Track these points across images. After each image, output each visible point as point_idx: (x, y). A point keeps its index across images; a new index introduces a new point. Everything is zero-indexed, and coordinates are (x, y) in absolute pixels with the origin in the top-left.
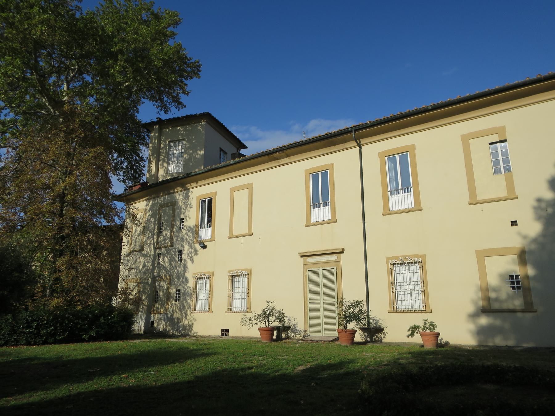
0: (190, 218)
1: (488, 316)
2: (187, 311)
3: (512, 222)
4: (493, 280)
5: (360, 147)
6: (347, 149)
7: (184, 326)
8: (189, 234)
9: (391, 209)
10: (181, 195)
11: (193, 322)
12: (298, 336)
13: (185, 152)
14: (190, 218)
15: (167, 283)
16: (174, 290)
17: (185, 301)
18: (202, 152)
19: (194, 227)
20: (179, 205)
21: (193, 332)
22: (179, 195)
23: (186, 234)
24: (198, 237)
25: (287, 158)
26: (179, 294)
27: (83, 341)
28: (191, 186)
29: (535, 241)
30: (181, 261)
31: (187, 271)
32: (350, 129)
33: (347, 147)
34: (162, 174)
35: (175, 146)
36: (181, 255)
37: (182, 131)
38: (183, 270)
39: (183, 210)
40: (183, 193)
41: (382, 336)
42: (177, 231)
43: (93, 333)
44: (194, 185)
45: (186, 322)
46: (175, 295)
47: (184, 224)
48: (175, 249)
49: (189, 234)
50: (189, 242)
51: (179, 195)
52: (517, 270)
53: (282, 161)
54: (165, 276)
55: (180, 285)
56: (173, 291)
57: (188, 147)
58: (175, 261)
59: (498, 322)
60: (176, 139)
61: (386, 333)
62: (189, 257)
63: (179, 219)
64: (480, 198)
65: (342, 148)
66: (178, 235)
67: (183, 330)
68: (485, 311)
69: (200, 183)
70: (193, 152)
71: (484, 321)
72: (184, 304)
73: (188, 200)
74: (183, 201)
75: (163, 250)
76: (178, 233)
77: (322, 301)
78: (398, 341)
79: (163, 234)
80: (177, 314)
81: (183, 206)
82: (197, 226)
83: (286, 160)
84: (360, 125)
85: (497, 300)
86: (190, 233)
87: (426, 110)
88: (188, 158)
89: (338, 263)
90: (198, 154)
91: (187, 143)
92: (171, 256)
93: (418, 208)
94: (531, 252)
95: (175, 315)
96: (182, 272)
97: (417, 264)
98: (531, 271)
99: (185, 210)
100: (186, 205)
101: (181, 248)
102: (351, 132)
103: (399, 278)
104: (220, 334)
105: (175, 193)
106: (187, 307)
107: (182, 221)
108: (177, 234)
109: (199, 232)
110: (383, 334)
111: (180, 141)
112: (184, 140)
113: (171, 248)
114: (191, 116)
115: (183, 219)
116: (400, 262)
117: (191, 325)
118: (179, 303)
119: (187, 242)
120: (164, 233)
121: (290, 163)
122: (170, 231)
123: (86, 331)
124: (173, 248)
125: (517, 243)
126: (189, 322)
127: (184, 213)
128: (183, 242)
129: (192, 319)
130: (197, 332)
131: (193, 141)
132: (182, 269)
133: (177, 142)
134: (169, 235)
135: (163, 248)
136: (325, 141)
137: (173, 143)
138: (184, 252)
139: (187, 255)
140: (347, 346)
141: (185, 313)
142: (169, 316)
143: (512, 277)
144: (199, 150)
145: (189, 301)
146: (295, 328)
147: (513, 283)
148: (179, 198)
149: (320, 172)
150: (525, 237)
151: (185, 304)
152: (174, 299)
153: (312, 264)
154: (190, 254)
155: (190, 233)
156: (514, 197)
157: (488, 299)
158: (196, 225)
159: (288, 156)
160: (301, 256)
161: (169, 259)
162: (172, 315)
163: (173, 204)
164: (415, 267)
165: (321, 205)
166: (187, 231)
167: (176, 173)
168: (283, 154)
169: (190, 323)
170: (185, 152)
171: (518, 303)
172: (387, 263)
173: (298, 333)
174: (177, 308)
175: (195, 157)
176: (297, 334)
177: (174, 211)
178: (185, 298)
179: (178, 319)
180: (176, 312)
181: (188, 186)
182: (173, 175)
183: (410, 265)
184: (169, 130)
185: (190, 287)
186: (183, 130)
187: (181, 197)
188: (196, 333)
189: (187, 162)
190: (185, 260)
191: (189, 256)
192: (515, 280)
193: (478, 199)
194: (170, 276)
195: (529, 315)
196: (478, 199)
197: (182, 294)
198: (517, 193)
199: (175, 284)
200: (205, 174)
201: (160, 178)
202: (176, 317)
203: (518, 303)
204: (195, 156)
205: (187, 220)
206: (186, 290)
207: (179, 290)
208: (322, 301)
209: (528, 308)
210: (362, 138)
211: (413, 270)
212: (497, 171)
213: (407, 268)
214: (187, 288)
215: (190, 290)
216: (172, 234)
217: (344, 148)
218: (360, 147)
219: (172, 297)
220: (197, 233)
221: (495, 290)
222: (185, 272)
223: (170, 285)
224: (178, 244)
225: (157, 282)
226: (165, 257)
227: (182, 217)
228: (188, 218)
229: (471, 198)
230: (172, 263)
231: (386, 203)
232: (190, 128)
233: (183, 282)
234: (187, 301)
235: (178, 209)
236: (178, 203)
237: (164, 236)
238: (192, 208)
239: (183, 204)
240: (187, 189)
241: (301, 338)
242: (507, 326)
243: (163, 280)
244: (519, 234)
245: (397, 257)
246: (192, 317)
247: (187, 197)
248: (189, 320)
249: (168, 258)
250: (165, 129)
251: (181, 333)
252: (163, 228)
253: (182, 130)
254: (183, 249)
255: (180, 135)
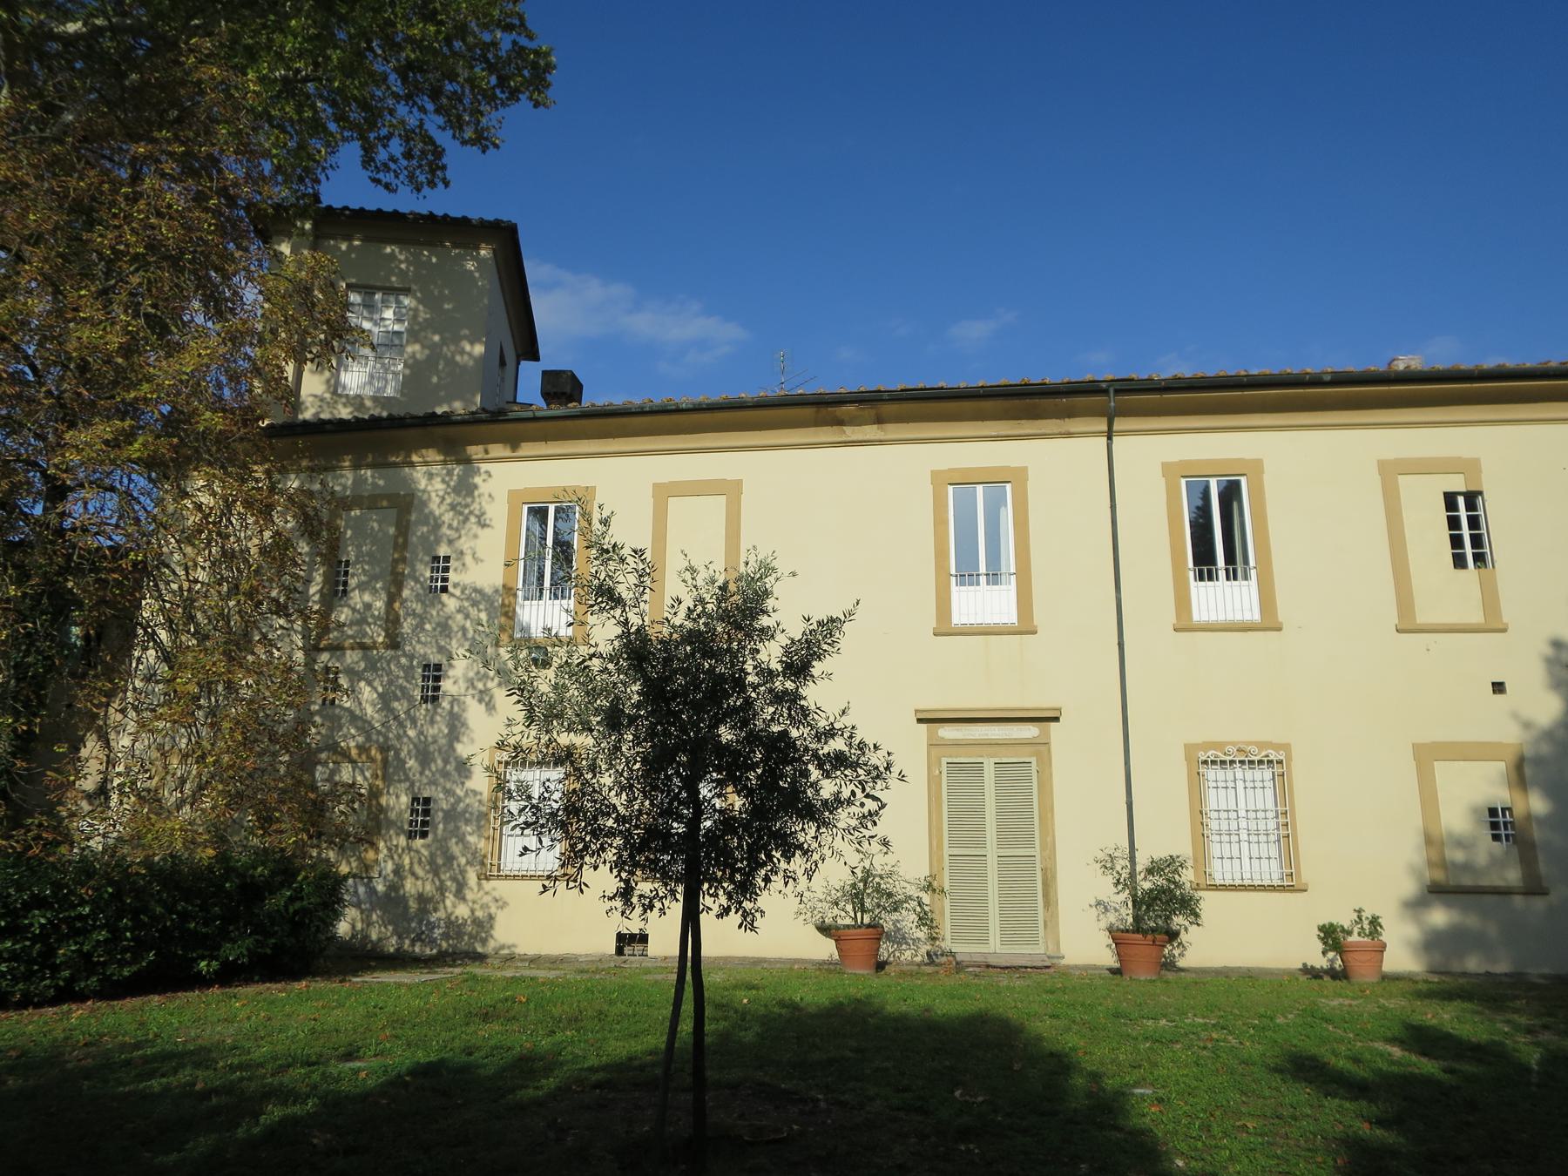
0: (476, 559)
1: (1448, 905)
2: (463, 872)
3: (1494, 684)
4: (1457, 818)
5: (1110, 438)
6: (1069, 435)
7: (450, 922)
8: (473, 612)
9: (1196, 618)
10: (439, 479)
11: (493, 910)
12: (908, 953)
13: (414, 335)
14: (476, 559)
15: (368, 774)
16: (405, 800)
17: (454, 840)
18: (479, 349)
19: (497, 591)
20: (427, 511)
21: (492, 944)
22: (430, 476)
23: (459, 611)
24: (513, 628)
25: (875, 426)
26: (426, 812)
27: (202, 982)
28: (486, 452)
29: (1548, 735)
30: (435, 699)
31: (465, 739)
32: (1104, 385)
33: (1073, 430)
34: (315, 393)
35: (369, 306)
36: (437, 679)
37: (401, 262)
38: (446, 731)
39: (445, 530)
40: (450, 473)
41: (1176, 952)
42: (418, 598)
43: (232, 952)
44: (497, 450)
45: (462, 911)
46: (407, 815)
47: (452, 575)
48: (411, 657)
49: (473, 612)
50: (473, 638)
51: (430, 476)
52: (1501, 795)
53: (851, 433)
54: (358, 747)
55: (433, 782)
56: (398, 802)
57: (426, 320)
58: (410, 699)
59: (1472, 921)
60: (378, 284)
61: (1186, 944)
62: (471, 691)
63: (427, 558)
64: (1422, 618)
65: (1056, 431)
66: (425, 612)
67: (446, 936)
68: (1437, 892)
69: (527, 449)
70: (444, 341)
71: (1439, 917)
72: (448, 849)
73: (469, 500)
74: (448, 500)
75: (352, 657)
76: (423, 603)
77: (992, 851)
78: (1238, 965)
79: (351, 602)
80: (419, 883)
81: (447, 517)
82: (509, 590)
83: (871, 431)
84: (1133, 380)
85: (1466, 867)
86: (479, 611)
87: (1316, 381)
88: (424, 357)
89: (1041, 747)
90: (462, 352)
91: (421, 308)
92: (390, 682)
93: (1269, 623)
94: (1538, 761)
95: (410, 886)
96: (443, 741)
97: (1265, 766)
98: (1537, 804)
99: (457, 530)
100: (461, 513)
101: (435, 658)
102: (1105, 392)
103: (1215, 799)
104: (610, 947)
105: (412, 465)
106: (463, 861)
107: (441, 565)
108: (419, 608)
109: (518, 609)
110: (1178, 947)
111: (389, 290)
112: (406, 291)
113: (389, 653)
114: (464, 222)
115: (447, 559)
116: (1228, 758)
117: (486, 919)
118: (427, 846)
119: (467, 639)
120: (357, 598)
121: (881, 442)
122: (384, 596)
123: (210, 946)
124: (400, 653)
125: (1511, 735)
126: (473, 911)
127: (450, 542)
128: (449, 636)
129: (487, 899)
130: (514, 946)
131: (446, 306)
132: (440, 730)
133: (378, 296)
134: (379, 610)
135: (352, 649)
136: (1016, 402)
137: (359, 293)
138: (451, 673)
139: (462, 685)
140: (1151, 981)
141: (453, 879)
142: (380, 888)
143: (1493, 812)
144: (466, 337)
145: (472, 839)
146: (899, 929)
147: (1494, 826)
148: (429, 488)
149: (981, 486)
150: (1527, 725)
151: (456, 849)
152: (403, 831)
153: (957, 744)
154: (480, 680)
155: (479, 611)
156: (1501, 627)
157: (1444, 864)
158: (504, 586)
159: (879, 420)
160: (920, 721)
161: (380, 689)
162: (394, 887)
163: (405, 505)
164: (1258, 774)
165: (983, 579)
166: (466, 604)
167: (375, 399)
168: (868, 411)
169: (479, 914)
170: (414, 335)
171: (1512, 876)
172: (1188, 759)
173: (907, 943)
174: (416, 860)
175: (451, 362)
176: (904, 947)
177: (404, 529)
178: (458, 828)
179: (422, 898)
180: (413, 874)
181: (475, 451)
182: (362, 405)
183: (1247, 767)
184: (350, 247)
185: (475, 793)
186: (407, 260)
187: (438, 485)
188: (509, 947)
189: (417, 374)
190: (454, 700)
191: (474, 687)
192: (1501, 819)
193: (1418, 622)
194: (384, 749)
195: (1539, 903)
196: (1418, 622)
197: (440, 814)
198: (1505, 620)
199: (407, 779)
200: (569, 423)
201: (308, 404)
202: (413, 891)
203: (1512, 876)
204: (453, 357)
205: (464, 565)
206: (459, 800)
207: (427, 801)
208: (992, 851)
209: (1534, 888)
210: (1119, 416)
211: (1254, 781)
212: (1459, 562)
213: (1239, 774)
214: (467, 794)
215: (480, 801)
216: (397, 605)
217: (1063, 431)
218: (1110, 438)
219: (391, 824)
220: (509, 613)
221: (1460, 843)
222: (458, 740)
223: (384, 779)
224: (425, 644)
225: (319, 768)
226: (362, 684)
227: (443, 551)
228: (468, 559)
229: (1401, 615)
230: (396, 705)
231: (1183, 602)
232: (434, 260)
233: (446, 775)
234: (461, 839)
235: (426, 523)
236: (424, 504)
237: (354, 610)
238: (486, 530)
239: (447, 511)
240: (467, 461)
241: (918, 959)
242: (1492, 930)
243: (353, 762)
244: (1515, 716)
245: (1219, 746)
246: (487, 893)
247: (465, 488)
248: (474, 902)
249: (375, 689)
250: (334, 238)
251: (440, 945)
252: (353, 582)
253: (402, 257)
254: (444, 661)
255: (395, 275)
